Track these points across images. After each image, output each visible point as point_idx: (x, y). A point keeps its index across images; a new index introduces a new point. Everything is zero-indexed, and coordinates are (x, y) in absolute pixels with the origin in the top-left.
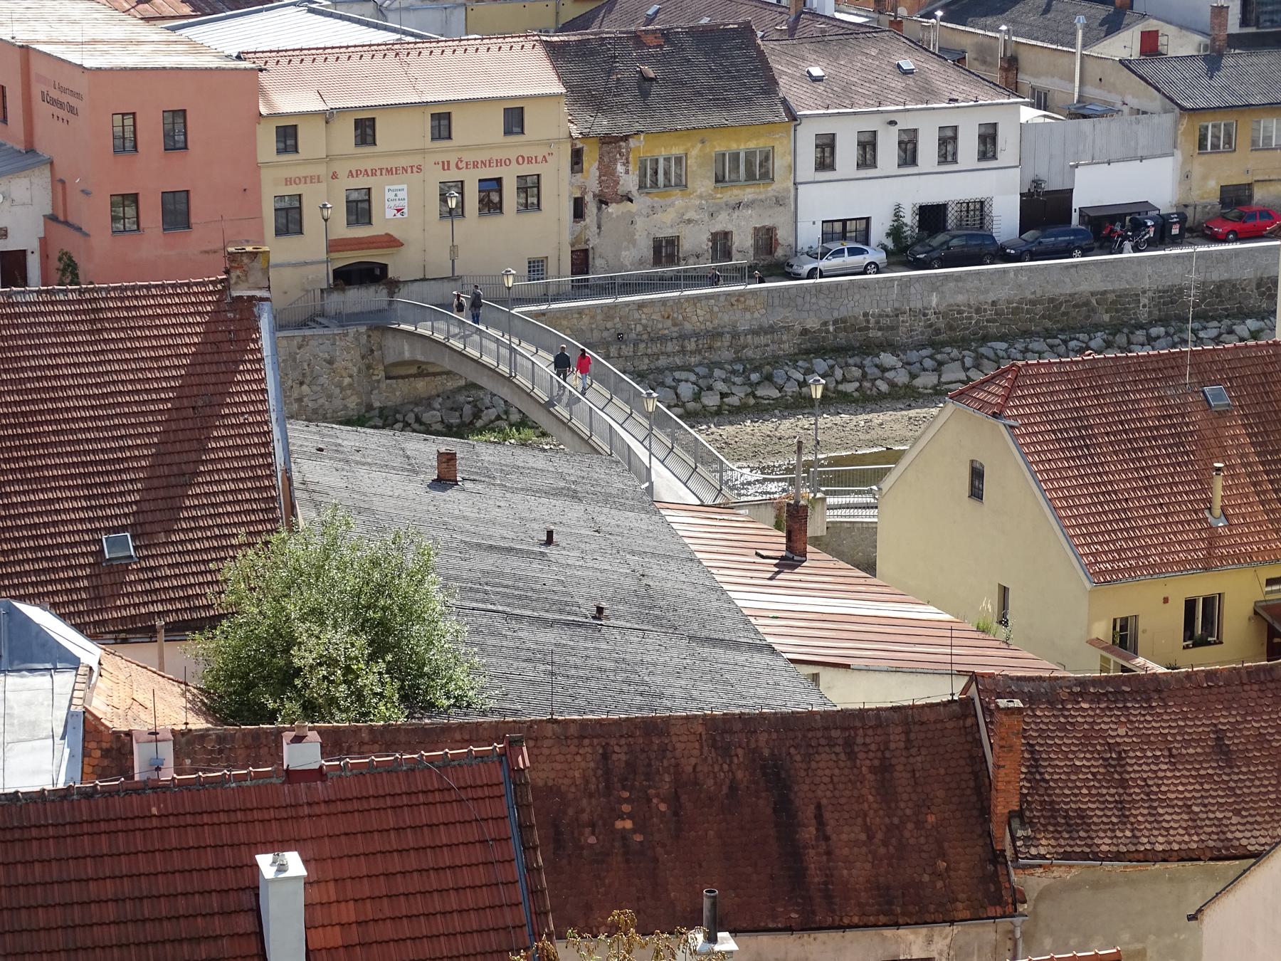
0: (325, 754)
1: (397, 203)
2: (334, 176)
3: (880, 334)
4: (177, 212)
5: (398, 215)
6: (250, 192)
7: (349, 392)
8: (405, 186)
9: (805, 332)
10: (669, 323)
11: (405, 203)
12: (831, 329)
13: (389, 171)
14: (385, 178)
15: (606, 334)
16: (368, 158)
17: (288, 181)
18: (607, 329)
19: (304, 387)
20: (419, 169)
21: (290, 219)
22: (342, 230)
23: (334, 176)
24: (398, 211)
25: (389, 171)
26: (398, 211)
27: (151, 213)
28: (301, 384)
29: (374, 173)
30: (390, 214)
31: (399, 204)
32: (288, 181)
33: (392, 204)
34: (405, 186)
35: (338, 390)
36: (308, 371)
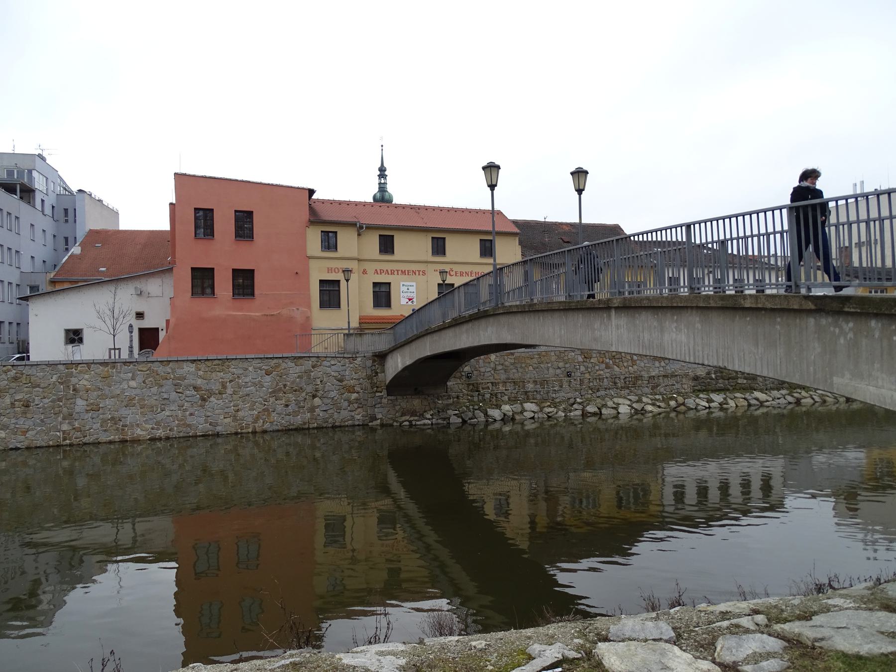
0: (786, 291)
1: (409, 294)
2: (365, 272)
3: (745, 381)
4: (244, 282)
5: (410, 303)
6: (300, 275)
7: (356, 405)
8: (414, 284)
9: (696, 378)
10: (603, 366)
11: (414, 295)
12: (713, 376)
13: (403, 272)
14: (400, 277)
15: (558, 371)
16: (386, 263)
17: (330, 270)
18: (559, 368)
19: (317, 399)
20: (424, 273)
21: (330, 294)
22: (371, 311)
23: (365, 272)
24: (410, 300)
25: (403, 272)
26: (410, 300)
27: (223, 284)
28: (314, 396)
29: (392, 273)
30: (404, 301)
31: (410, 295)
32: (330, 270)
33: (405, 295)
34: (414, 284)
35: (346, 404)
36: (320, 387)
